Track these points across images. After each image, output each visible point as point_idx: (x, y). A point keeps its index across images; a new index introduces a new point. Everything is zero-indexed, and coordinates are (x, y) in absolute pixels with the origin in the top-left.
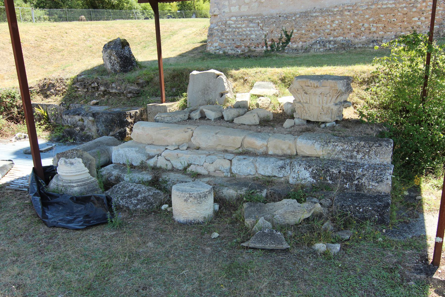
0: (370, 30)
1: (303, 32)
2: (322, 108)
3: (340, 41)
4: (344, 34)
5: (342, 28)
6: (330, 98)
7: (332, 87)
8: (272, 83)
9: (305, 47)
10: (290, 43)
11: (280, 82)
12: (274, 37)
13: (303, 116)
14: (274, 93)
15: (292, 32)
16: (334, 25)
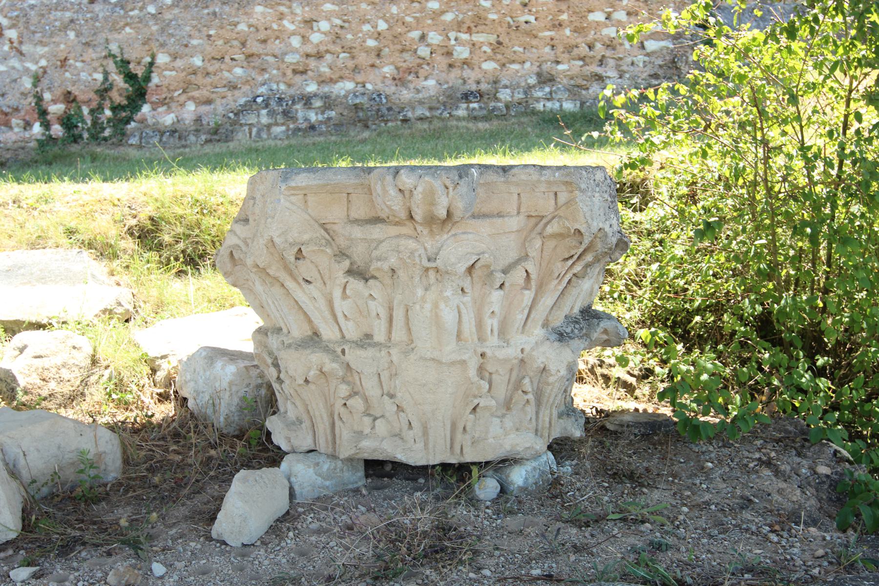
0: (449, 54)
1: (197, 62)
2: (481, 369)
3: (346, 97)
4: (356, 69)
5: (349, 49)
6: (529, 295)
7: (538, 220)
8: (86, 254)
9: (210, 121)
10: (146, 109)
11: (130, 244)
12: (74, 83)
13: (344, 433)
14: (109, 303)
15: (151, 64)
16: (316, 38)
